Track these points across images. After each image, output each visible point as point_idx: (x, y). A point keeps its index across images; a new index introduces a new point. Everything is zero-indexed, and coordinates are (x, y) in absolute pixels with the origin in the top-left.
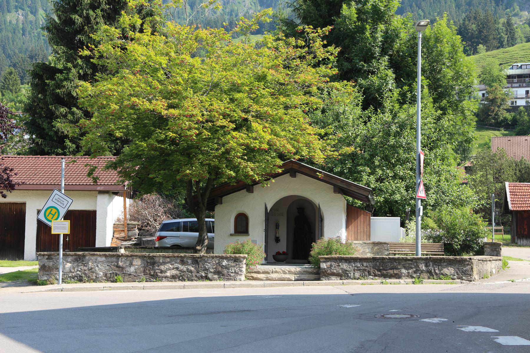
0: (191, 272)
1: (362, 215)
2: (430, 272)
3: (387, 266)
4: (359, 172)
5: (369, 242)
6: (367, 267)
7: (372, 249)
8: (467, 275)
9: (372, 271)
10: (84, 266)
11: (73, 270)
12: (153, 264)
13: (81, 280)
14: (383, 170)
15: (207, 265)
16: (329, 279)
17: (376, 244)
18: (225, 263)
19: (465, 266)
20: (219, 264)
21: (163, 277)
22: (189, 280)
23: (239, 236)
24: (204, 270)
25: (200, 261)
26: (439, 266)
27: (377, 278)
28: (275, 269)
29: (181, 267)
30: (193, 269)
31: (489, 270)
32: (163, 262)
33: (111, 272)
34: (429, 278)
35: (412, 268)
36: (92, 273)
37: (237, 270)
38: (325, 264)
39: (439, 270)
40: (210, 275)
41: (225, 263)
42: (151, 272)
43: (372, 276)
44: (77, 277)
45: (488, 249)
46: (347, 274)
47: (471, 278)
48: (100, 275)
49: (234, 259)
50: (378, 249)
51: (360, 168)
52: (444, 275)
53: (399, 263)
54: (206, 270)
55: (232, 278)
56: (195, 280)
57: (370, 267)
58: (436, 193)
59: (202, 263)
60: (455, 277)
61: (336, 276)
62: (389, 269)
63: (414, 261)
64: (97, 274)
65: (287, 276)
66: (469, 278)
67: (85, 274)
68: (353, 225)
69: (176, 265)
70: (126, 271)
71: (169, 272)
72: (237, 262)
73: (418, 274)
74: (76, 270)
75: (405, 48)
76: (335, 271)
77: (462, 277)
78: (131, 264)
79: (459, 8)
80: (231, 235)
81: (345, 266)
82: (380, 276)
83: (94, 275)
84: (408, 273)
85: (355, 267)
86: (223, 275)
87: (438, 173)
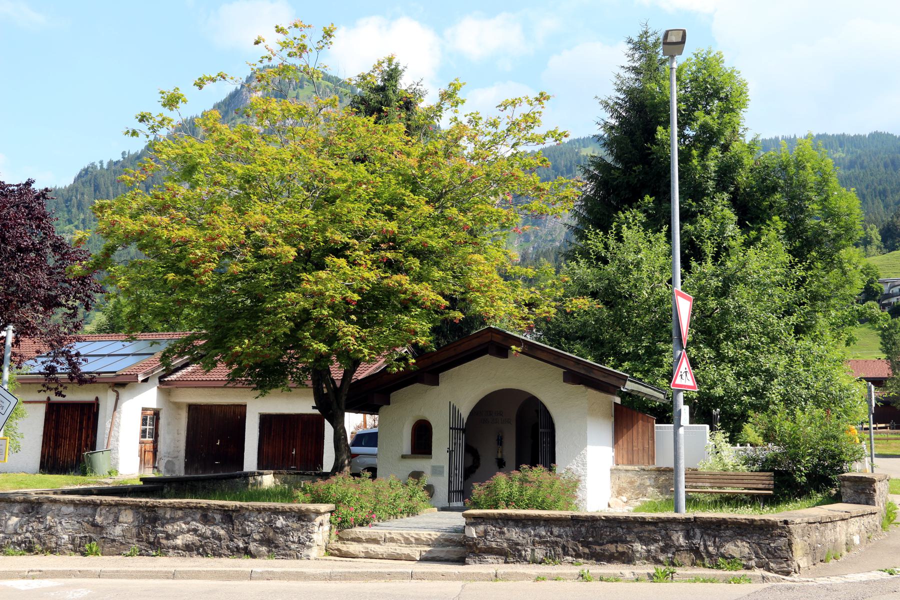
0: (219, 538)
1: (640, 422)
2: (696, 551)
3: (602, 535)
4: (661, 352)
5: (651, 467)
6: (559, 536)
7: (656, 479)
8: (779, 560)
9: (570, 546)
10: (40, 522)
11: (19, 531)
12: (154, 520)
13: (30, 550)
14: (699, 349)
15: (248, 525)
16: (481, 562)
17: (663, 471)
18: (280, 522)
19: (773, 538)
20: (270, 524)
21: (169, 547)
22: (214, 555)
23: (423, 458)
24: (243, 536)
25: (237, 518)
26: (715, 537)
27: (581, 560)
28: (390, 533)
29: (202, 528)
30: (222, 532)
31: (843, 539)
32: (172, 518)
33: (82, 535)
34: (694, 564)
35: (656, 541)
36: (51, 537)
37: (303, 537)
38: (473, 530)
39: (715, 546)
40: (252, 547)
41: (280, 522)
42: (149, 537)
43: (572, 556)
44: (25, 542)
45: (849, 490)
46: (519, 551)
47: (788, 565)
48: (63, 541)
49: (297, 515)
50: (666, 480)
52: (727, 558)
53: (629, 530)
54: (247, 535)
55: (292, 552)
56: (225, 555)
57: (567, 536)
58: (786, 384)
59: (240, 522)
60: (753, 563)
61: (496, 554)
62: (607, 543)
63: (660, 525)
64: (59, 538)
65: (406, 550)
66: (785, 565)
67: (39, 538)
68: (625, 438)
69: (194, 524)
70: (107, 533)
71: (180, 537)
72: (304, 521)
73: (670, 555)
74: (24, 531)
75: (754, 183)
76: (494, 545)
77: (768, 564)
78: (116, 521)
79: (887, 208)
81: (514, 534)
82: (588, 557)
83: (54, 539)
84: (649, 551)
85: (535, 536)
86: (277, 547)
87: (790, 352)
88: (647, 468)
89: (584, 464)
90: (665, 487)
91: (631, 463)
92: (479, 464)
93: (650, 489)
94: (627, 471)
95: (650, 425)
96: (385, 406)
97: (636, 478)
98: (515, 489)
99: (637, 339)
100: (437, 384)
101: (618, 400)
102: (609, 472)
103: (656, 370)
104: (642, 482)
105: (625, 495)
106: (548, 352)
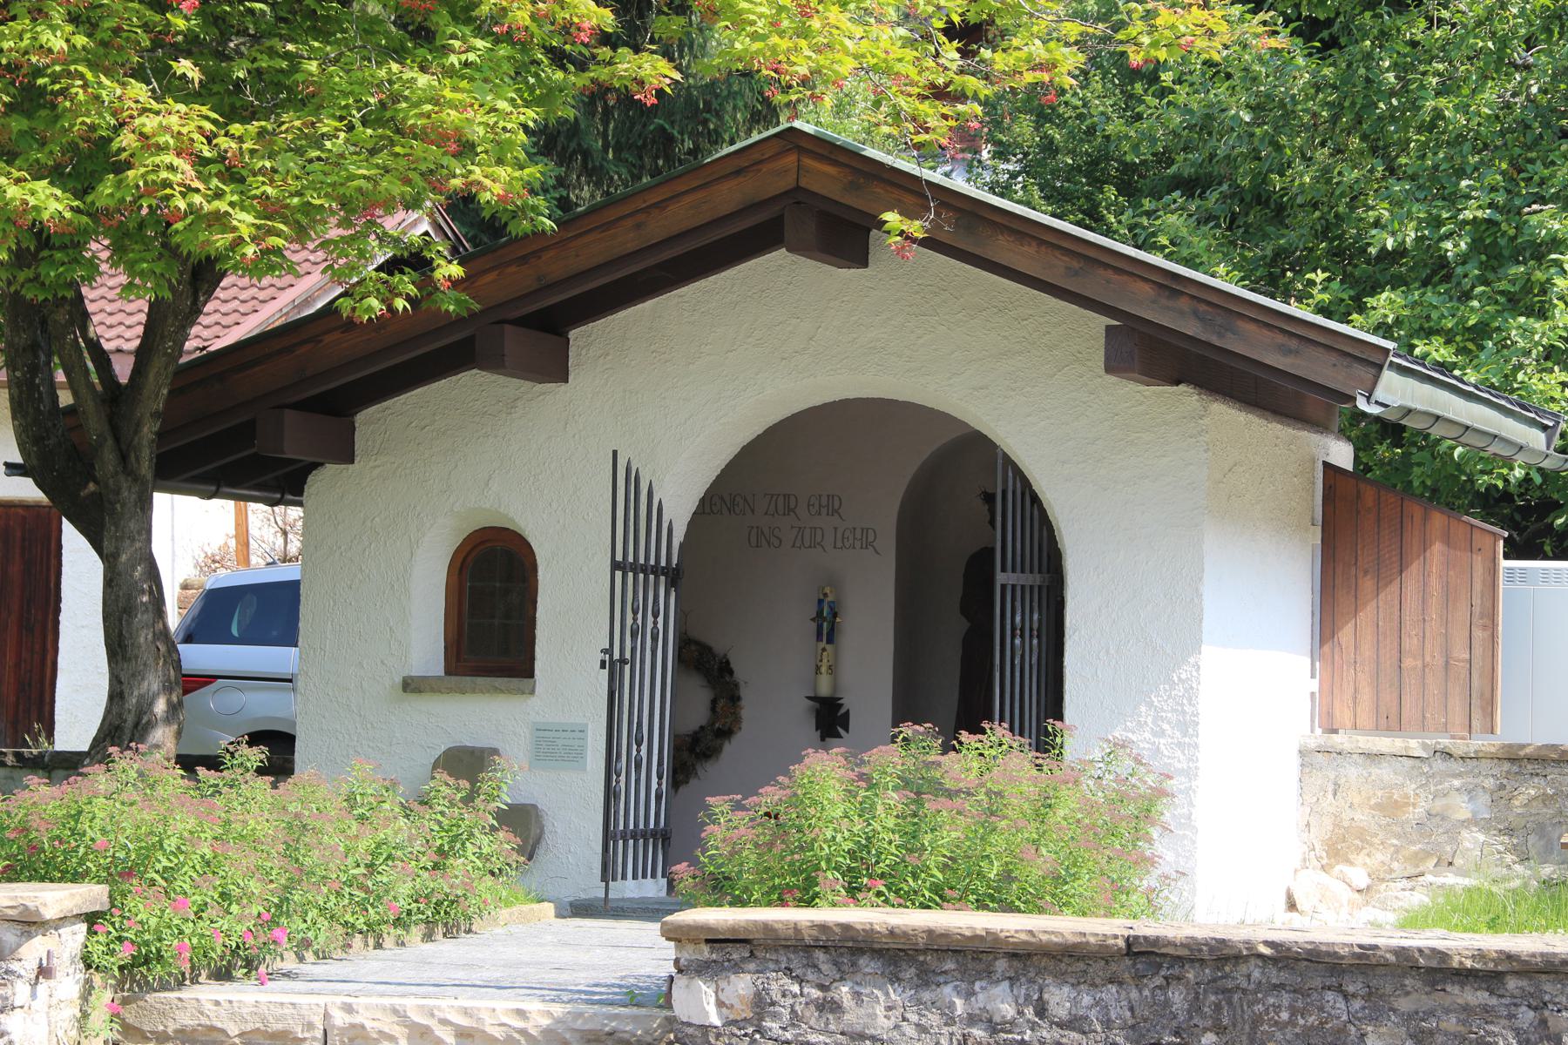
1: (1437, 548)
3: (1257, 1021)
7: (1500, 796)
28: (348, 1009)
50: (1545, 799)
57: (1108, 1024)
63: (1512, 984)
68: (1366, 615)
80: (411, 686)
85: (972, 1020)
88: (1460, 747)
89: (1188, 725)
91: (1392, 723)
92: (737, 720)
93: (1472, 840)
95: (1478, 560)
96: (330, 470)
97: (1411, 788)
98: (886, 821)
102: (1295, 761)
104: (1439, 804)
105: (1360, 859)
106: (1042, 242)
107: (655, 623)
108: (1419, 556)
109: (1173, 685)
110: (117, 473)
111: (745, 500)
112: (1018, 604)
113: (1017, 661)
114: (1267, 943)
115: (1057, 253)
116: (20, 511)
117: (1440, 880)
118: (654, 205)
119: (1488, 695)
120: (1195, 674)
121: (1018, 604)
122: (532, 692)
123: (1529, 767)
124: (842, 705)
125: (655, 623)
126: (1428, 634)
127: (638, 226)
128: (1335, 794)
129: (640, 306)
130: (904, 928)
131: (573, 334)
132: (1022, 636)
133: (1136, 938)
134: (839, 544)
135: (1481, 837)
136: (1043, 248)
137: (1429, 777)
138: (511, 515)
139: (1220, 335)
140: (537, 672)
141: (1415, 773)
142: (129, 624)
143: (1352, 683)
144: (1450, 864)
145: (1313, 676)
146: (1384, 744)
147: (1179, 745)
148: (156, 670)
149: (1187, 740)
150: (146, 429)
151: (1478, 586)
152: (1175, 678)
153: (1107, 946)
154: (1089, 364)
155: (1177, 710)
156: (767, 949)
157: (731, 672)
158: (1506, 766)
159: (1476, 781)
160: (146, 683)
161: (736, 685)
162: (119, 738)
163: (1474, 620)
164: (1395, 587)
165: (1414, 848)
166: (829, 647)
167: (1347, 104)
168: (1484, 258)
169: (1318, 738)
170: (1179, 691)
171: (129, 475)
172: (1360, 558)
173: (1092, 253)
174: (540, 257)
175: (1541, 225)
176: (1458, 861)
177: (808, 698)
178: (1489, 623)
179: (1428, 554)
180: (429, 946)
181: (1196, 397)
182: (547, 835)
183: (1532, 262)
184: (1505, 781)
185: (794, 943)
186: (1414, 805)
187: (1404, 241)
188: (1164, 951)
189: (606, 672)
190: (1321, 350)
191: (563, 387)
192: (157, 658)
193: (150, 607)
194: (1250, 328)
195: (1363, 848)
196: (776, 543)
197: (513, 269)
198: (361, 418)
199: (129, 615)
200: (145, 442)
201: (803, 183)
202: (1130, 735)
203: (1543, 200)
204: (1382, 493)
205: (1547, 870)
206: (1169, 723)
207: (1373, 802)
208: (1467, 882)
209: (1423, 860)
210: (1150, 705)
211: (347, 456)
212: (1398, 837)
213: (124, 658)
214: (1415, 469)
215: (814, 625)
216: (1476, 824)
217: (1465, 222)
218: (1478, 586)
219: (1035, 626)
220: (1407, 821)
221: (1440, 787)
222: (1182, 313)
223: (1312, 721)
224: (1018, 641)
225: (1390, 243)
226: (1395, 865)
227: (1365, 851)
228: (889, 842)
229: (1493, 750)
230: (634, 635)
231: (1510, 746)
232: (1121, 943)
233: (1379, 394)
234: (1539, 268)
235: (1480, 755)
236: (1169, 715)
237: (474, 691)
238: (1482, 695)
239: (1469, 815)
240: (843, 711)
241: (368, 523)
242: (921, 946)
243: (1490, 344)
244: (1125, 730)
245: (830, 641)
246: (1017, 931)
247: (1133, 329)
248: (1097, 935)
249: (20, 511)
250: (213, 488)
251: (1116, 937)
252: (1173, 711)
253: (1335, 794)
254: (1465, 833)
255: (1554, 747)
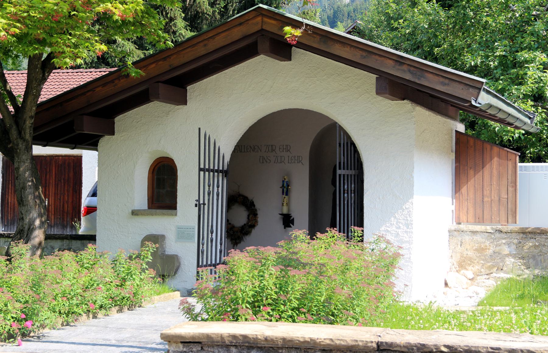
1: (496, 159)
4: (521, 65)
5: (511, 227)
7: (519, 245)
23: (164, 214)
50: (535, 247)
51: (524, 55)
68: (471, 183)
80: (135, 213)
88: (505, 228)
89: (409, 225)
90: (534, 257)
91: (480, 220)
92: (256, 222)
93: (510, 261)
94: (474, 232)
95: (510, 163)
96: (107, 138)
97: (488, 243)
98: (270, 282)
99: (488, 46)
100: (184, 102)
101: (461, 128)
102: (448, 234)
103: (514, 89)
104: (498, 249)
105: (470, 268)
106: (352, 46)
107: (218, 190)
108: (489, 162)
109: (403, 210)
110: (17, 138)
111: (258, 147)
112: (346, 181)
113: (346, 202)
114: (445, 346)
115: (357, 50)
116: (73, 158)
117: (498, 275)
118: (211, 37)
119: (514, 210)
120: (411, 206)
121: (346, 181)
122: (176, 215)
123: (529, 235)
124: (291, 216)
125: (218, 190)
126: (492, 189)
127: (205, 45)
128: (461, 246)
129: (211, 77)
130: (272, 337)
131: (188, 88)
132: (348, 193)
133: (382, 343)
134: (290, 162)
135: (513, 260)
136: (352, 48)
137: (494, 239)
138: (168, 152)
139: (419, 79)
140: (178, 208)
141: (489, 238)
142: (24, 193)
143: (466, 207)
144: (502, 269)
145: (453, 204)
146: (478, 228)
147: (406, 232)
148: (35, 209)
149: (408, 230)
150: (27, 122)
151: (510, 172)
152: (404, 208)
153: (368, 347)
154: (371, 93)
155: (404, 219)
156: (209, 346)
157: (254, 206)
158: (521, 235)
159: (511, 240)
160: (32, 214)
161: (256, 210)
162: (23, 234)
163: (509, 184)
164: (481, 173)
165: (489, 264)
166: (286, 197)
167: (458, 22)
168: (502, 68)
169: (455, 226)
170: (406, 212)
171: (21, 139)
172: (468, 163)
173: (370, 49)
174: (170, 58)
175: (522, 56)
176: (505, 269)
177: (280, 214)
178: (514, 185)
179: (492, 161)
180: (120, 315)
181: (411, 105)
182: (182, 266)
183: (519, 68)
184: (521, 241)
185: (221, 343)
186: (489, 249)
187: (477, 63)
188: (395, 349)
189: (197, 208)
190: (457, 83)
191: (185, 107)
192: (36, 205)
193: (32, 187)
194: (430, 76)
195: (471, 264)
196: (269, 161)
197: (161, 63)
198: (117, 119)
199: (24, 189)
200: (27, 127)
201: (264, 28)
202: (388, 228)
203: (522, 49)
204: (476, 140)
205: (537, 272)
206: (402, 224)
207: (474, 248)
208: (508, 276)
209: (492, 268)
210: (395, 217)
211: (113, 133)
212: (483, 260)
213: (23, 205)
214: (482, 135)
215: (281, 189)
216: (511, 255)
217: (496, 56)
218: (510, 172)
219: (353, 189)
220: (487, 255)
221: (498, 243)
222: (404, 71)
223: (453, 220)
224: (346, 195)
225: (473, 64)
226: (482, 270)
227: (472, 265)
228: (272, 292)
229: (517, 230)
230: (209, 194)
231: (523, 228)
232: (375, 345)
233: (480, 100)
234: (521, 70)
235: (512, 231)
236: (402, 221)
237: (156, 215)
238: (512, 210)
239: (508, 253)
240: (292, 218)
241: (120, 156)
242: (280, 346)
243: (506, 94)
244: (386, 227)
245: (287, 195)
246: (325, 339)
247: (386, 78)
248: (363, 341)
249: (73, 158)
250: (74, 146)
251: (372, 342)
252: (404, 219)
253: (461, 246)
254: (507, 259)
255: (538, 228)
